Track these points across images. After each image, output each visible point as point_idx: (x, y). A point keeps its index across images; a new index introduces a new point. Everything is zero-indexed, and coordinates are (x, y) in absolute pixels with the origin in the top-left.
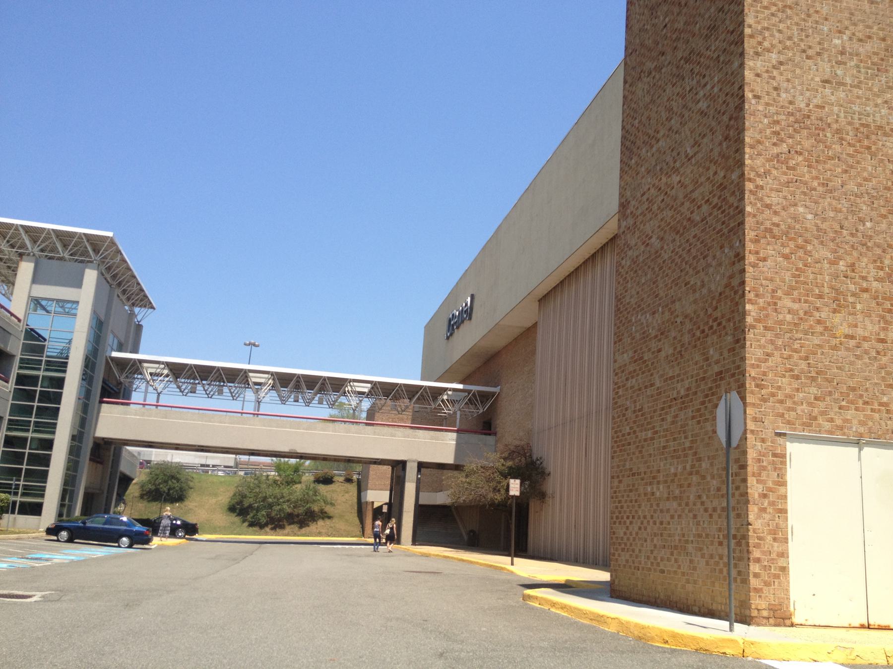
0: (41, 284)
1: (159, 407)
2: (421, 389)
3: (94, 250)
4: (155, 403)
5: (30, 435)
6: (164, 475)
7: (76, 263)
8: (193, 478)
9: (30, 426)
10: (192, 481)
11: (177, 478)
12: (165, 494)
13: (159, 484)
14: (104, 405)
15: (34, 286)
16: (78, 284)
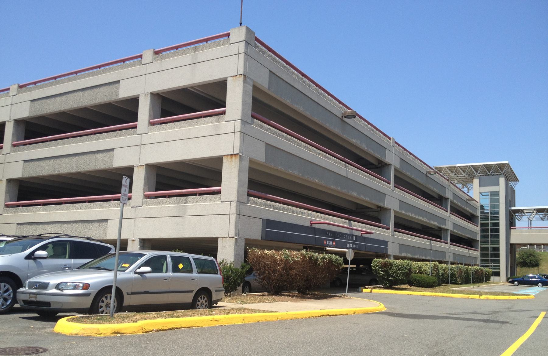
0: (482, 187)
1: (532, 229)
2: (545, 210)
3: (475, 170)
4: (528, 227)
5: (490, 246)
6: (527, 254)
7: (496, 176)
8: (541, 254)
9: (489, 242)
10: (540, 256)
11: (533, 255)
12: (529, 264)
13: (525, 259)
14: (512, 230)
15: (480, 188)
16: (498, 184)
